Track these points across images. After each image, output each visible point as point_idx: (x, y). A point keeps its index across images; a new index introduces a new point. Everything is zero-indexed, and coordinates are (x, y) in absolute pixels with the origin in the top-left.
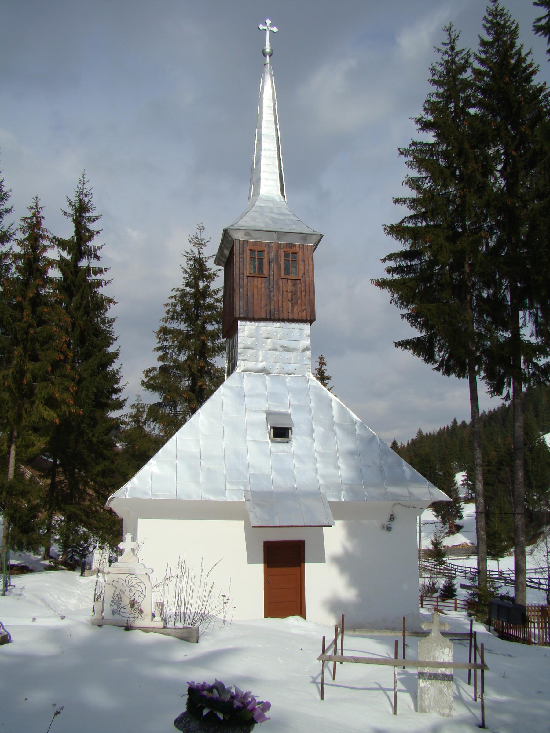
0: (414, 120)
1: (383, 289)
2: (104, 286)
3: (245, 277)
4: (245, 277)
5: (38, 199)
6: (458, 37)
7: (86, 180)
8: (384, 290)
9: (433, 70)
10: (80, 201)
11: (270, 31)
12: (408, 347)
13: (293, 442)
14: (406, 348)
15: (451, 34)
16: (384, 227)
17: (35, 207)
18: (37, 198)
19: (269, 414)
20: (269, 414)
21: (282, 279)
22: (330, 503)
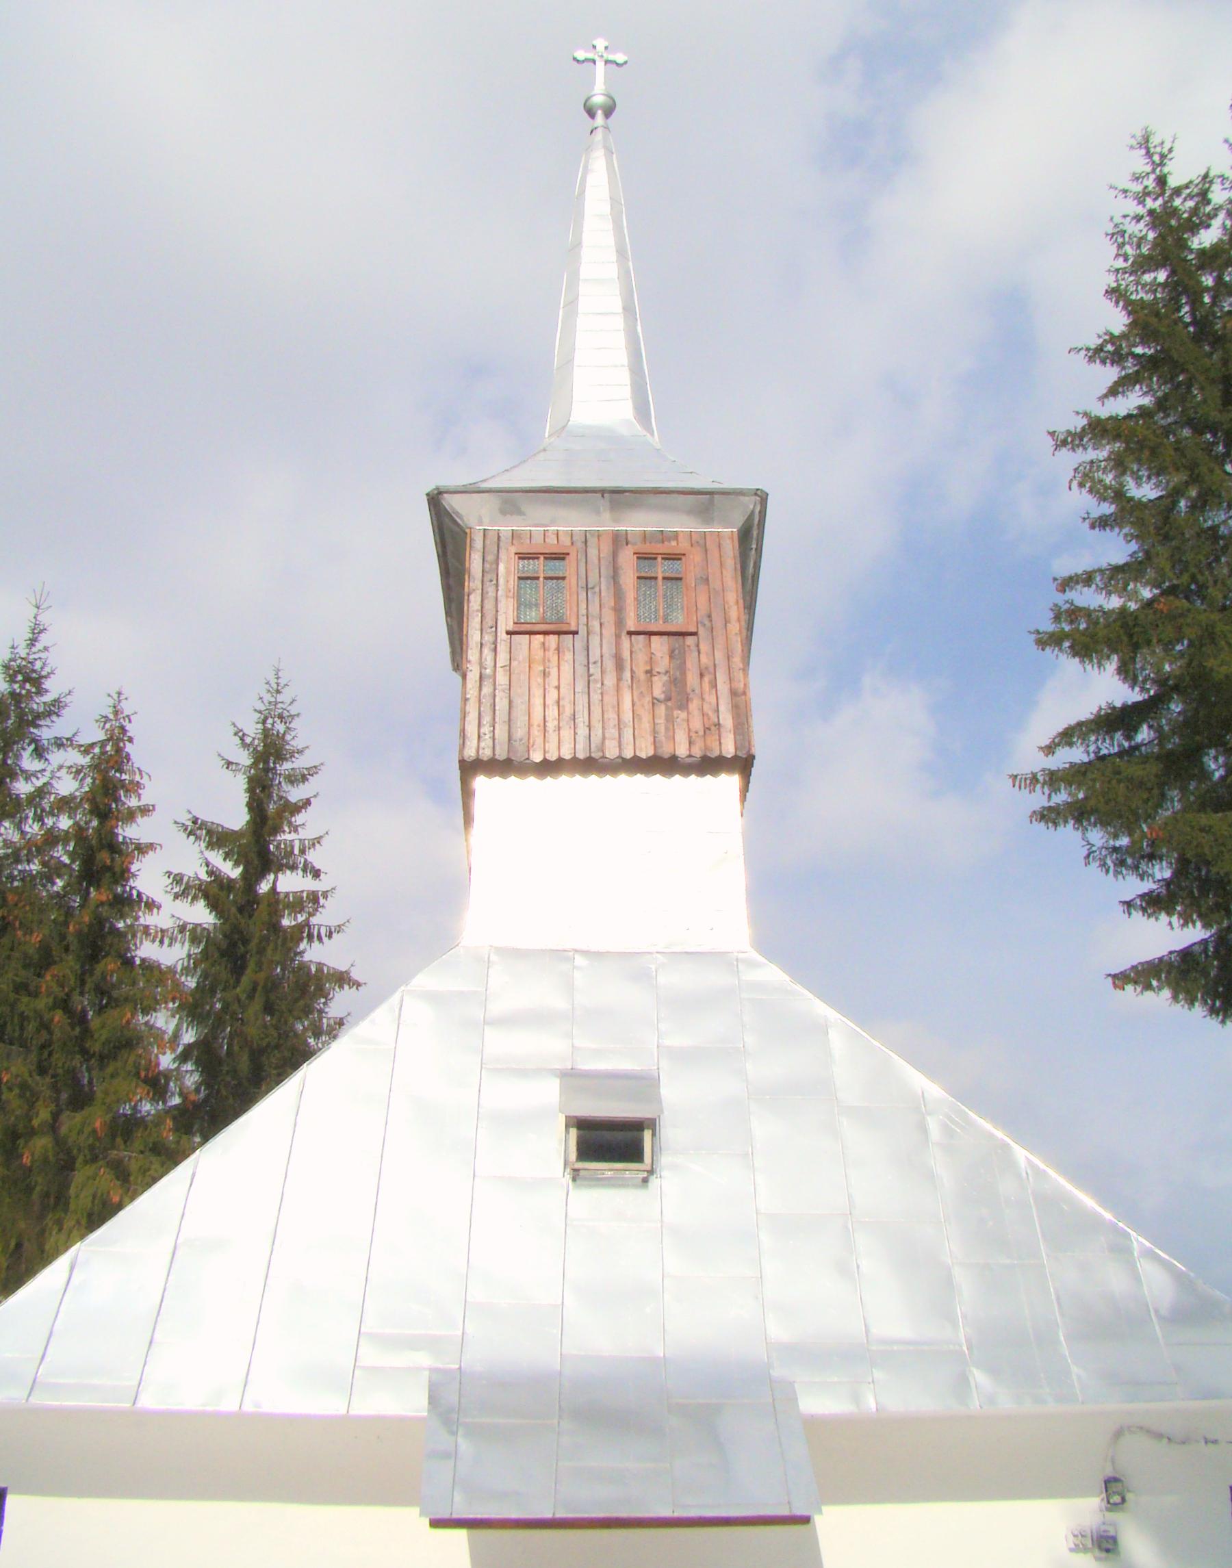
0: (1083, 353)
1: (1055, 824)
2: (325, 939)
3: (502, 635)
4: (502, 635)
5: (122, 697)
6: (1170, 150)
7: (282, 682)
8: (1061, 828)
9: (1118, 234)
10: (266, 733)
11: (607, 62)
12: (1154, 983)
13: (668, 1182)
14: (1148, 987)
15: (1152, 150)
16: (1033, 637)
17: (111, 716)
18: (119, 694)
19: (571, 1078)
20: (571, 1078)
21: (630, 633)
22: (814, 1425)
